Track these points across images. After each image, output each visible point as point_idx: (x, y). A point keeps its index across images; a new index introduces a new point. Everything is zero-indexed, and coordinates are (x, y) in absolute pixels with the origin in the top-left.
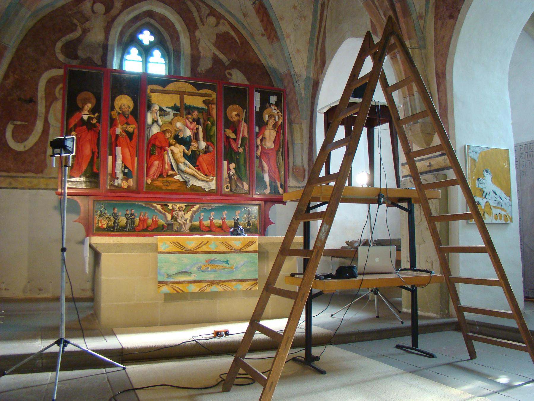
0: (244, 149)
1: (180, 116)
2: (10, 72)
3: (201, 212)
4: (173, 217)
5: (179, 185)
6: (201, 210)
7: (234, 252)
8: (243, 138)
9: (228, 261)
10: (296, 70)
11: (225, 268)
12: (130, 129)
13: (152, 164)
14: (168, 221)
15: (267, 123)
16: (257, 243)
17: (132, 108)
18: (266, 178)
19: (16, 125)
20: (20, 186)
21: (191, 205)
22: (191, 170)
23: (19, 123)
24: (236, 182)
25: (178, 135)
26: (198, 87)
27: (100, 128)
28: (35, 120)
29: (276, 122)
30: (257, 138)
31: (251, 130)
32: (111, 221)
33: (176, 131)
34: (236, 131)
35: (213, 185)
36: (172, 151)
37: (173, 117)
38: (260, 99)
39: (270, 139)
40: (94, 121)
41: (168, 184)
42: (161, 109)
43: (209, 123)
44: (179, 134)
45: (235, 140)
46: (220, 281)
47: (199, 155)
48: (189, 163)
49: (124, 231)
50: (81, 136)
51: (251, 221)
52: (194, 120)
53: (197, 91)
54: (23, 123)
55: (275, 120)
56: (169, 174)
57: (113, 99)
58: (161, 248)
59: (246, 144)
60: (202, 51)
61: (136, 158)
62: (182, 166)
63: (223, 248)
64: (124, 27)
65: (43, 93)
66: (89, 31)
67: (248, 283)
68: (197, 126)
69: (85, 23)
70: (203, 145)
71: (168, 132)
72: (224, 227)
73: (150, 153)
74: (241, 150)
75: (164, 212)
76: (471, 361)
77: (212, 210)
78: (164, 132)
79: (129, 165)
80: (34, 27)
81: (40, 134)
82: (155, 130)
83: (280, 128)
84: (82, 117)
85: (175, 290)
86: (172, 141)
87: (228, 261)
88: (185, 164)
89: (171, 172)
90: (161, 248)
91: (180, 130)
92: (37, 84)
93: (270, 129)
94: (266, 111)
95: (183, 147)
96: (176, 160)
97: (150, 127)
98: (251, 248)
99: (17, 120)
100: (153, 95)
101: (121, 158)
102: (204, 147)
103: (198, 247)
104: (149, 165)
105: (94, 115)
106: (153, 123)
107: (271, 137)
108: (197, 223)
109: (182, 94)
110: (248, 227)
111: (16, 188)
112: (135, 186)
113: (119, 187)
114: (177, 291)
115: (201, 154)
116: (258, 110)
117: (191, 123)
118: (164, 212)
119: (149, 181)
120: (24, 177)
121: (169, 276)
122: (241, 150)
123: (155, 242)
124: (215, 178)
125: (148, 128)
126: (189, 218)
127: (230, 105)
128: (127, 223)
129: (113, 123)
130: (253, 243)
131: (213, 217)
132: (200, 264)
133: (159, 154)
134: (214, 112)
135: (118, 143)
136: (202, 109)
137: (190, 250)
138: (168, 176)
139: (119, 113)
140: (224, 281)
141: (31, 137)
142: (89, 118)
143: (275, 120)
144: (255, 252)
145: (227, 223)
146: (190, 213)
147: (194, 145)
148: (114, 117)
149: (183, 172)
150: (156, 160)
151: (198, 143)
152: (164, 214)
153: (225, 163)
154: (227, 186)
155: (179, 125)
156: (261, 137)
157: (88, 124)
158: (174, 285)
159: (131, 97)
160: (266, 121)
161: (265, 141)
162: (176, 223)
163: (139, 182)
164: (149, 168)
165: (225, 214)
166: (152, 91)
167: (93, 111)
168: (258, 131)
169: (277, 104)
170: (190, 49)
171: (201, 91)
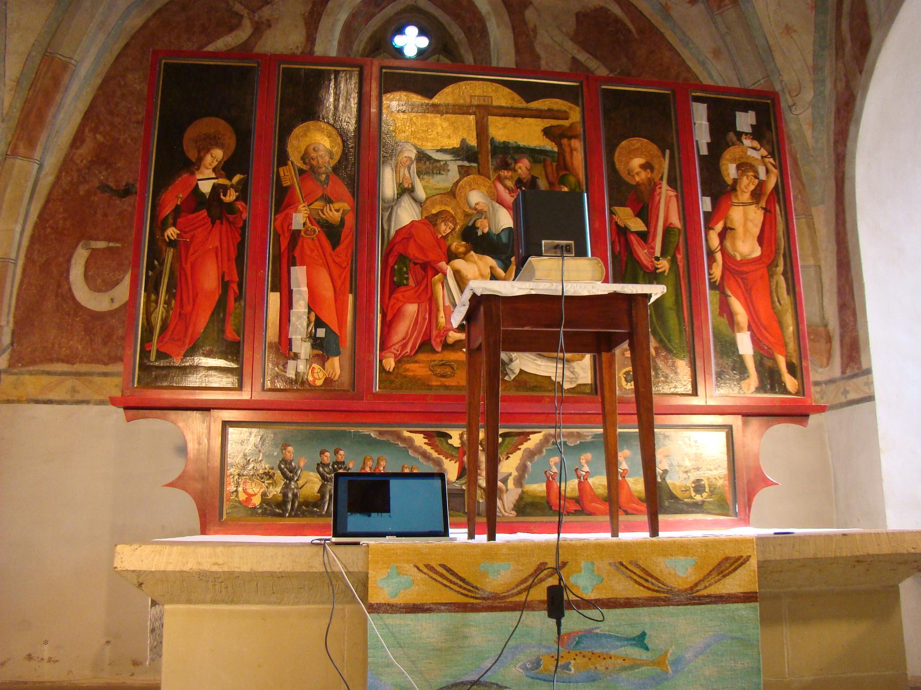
0: (674, 262)
1: (479, 173)
2: (87, 130)
3: (551, 453)
6: (550, 446)
7: (667, 602)
9: (643, 635)
10: (785, 78)
11: (635, 665)
12: (333, 214)
15: (734, 187)
16: (753, 563)
17: (337, 158)
18: (745, 344)
19: (93, 250)
20: (96, 397)
23: (101, 245)
26: (528, 92)
27: (245, 215)
29: (761, 185)
30: (708, 228)
31: (688, 208)
32: (274, 484)
33: (467, 215)
34: (645, 211)
36: (457, 274)
38: (709, 120)
39: (746, 230)
40: (231, 196)
41: (448, 371)
42: (422, 157)
44: (478, 224)
49: (313, 514)
50: (192, 238)
53: (524, 105)
54: (111, 244)
55: (756, 177)
56: (450, 340)
57: (285, 132)
58: (383, 589)
59: (677, 248)
60: (543, 55)
61: (351, 297)
63: (623, 588)
64: (354, 16)
66: (270, 26)
69: (260, 8)
73: (392, 281)
75: (435, 455)
78: (431, 221)
79: (330, 318)
80: (145, 26)
82: (407, 215)
83: (776, 201)
84: (197, 185)
86: (457, 245)
87: (643, 635)
90: (383, 589)
91: (481, 213)
93: (744, 204)
94: (728, 154)
97: (391, 206)
98: (733, 584)
99: (96, 240)
101: (306, 296)
105: (230, 180)
107: (750, 224)
108: (538, 488)
109: (483, 112)
111: (87, 402)
112: (346, 379)
113: (300, 382)
116: (704, 151)
118: (435, 455)
119: (390, 363)
120: (105, 374)
123: (357, 567)
126: (515, 473)
127: (625, 137)
128: (322, 490)
129: (284, 199)
130: (738, 562)
133: (418, 283)
134: (578, 160)
135: (297, 253)
136: (543, 152)
137: (495, 597)
138: (446, 346)
139: (301, 172)
143: (756, 177)
144: (748, 598)
148: (286, 183)
154: (627, 373)
155: (476, 198)
156: (719, 227)
157: (213, 205)
160: (730, 182)
161: (734, 239)
163: (360, 366)
164: (388, 326)
167: (226, 169)
168: (709, 209)
169: (758, 133)
170: (513, 51)
171: (535, 105)
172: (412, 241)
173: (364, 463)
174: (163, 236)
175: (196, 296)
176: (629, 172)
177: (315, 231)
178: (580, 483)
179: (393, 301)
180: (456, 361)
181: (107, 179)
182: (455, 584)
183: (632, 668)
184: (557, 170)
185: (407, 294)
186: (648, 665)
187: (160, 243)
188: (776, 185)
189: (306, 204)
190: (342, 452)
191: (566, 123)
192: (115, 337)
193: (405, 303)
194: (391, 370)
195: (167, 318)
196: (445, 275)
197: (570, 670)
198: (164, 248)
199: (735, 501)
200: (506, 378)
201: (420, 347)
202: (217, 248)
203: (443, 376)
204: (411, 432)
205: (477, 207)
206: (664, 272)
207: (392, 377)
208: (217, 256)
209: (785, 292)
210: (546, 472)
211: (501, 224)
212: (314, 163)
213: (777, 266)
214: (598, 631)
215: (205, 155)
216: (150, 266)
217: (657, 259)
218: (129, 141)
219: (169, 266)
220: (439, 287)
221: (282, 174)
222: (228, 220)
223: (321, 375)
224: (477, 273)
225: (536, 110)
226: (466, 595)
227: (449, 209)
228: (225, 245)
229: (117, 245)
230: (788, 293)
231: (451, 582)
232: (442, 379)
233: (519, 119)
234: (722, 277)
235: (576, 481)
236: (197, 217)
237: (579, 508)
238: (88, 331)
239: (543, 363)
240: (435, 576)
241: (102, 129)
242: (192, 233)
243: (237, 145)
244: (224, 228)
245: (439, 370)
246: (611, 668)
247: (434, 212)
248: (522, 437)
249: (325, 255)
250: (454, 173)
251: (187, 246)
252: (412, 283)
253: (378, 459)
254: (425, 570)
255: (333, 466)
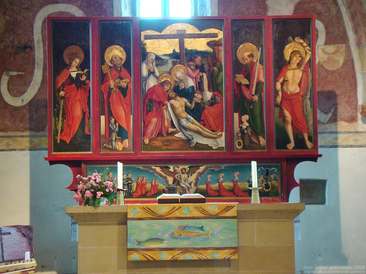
3: (208, 174)
4: (174, 181)
5: (181, 143)
7: (210, 218)
8: (259, 83)
9: (202, 227)
12: (123, 84)
13: (149, 122)
14: (169, 185)
17: (124, 61)
20: (19, 147)
21: (196, 167)
22: (194, 125)
23: (14, 73)
24: (249, 137)
25: (178, 87)
28: (33, 69)
29: (303, 59)
33: (176, 82)
35: (222, 142)
36: (172, 105)
37: (172, 66)
40: (84, 78)
41: (169, 143)
43: (216, 68)
44: (180, 85)
45: (248, 86)
46: (195, 249)
47: (204, 108)
48: (192, 118)
50: (70, 95)
51: (269, 183)
52: (197, 67)
53: (199, 32)
54: (20, 73)
56: (169, 132)
59: (262, 90)
62: (184, 122)
65: (40, 36)
67: (226, 251)
68: (201, 74)
70: (208, 95)
71: (167, 84)
72: (236, 191)
73: (147, 109)
74: (256, 98)
75: (164, 175)
76: (126, 261)
77: (221, 171)
81: (39, 85)
82: (152, 83)
85: (146, 257)
87: (202, 227)
88: (187, 119)
89: (171, 130)
91: (181, 80)
92: (32, 26)
93: (293, 69)
95: (185, 100)
96: (177, 116)
98: (228, 214)
100: (148, 42)
102: (209, 98)
103: (170, 213)
104: (146, 123)
105: (83, 72)
106: (149, 75)
107: (295, 78)
110: (267, 190)
111: (15, 150)
114: (147, 259)
115: (206, 106)
117: (193, 70)
118: (164, 175)
120: (22, 136)
121: (139, 243)
122: (256, 98)
124: (224, 133)
125: (144, 81)
126: (194, 181)
131: (222, 179)
132: (173, 231)
133: (157, 110)
137: (162, 216)
138: (168, 134)
139: (110, 67)
140: (198, 249)
141: (29, 90)
142: (78, 75)
144: (234, 217)
145: (240, 187)
146: (194, 176)
147: (198, 96)
149: (186, 129)
150: (154, 117)
151: (202, 94)
152: (165, 178)
153: (236, 115)
156: (281, 80)
157: (78, 82)
158: (145, 252)
159: (123, 48)
161: (287, 85)
162: (179, 187)
164: (146, 127)
165: (222, 176)
166: (147, 37)
171: (204, 32)
172: (154, 92)
173: (138, 178)
174: (59, 95)
175: (73, 117)
176: (243, 59)
177: (117, 91)
178: (219, 185)
179: (147, 117)
180: (172, 140)
181: (14, 39)
182: (150, 212)
183: (199, 236)
184: (213, 60)
185: (153, 115)
186: (204, 235)
187: (58, 98)
188: (310, 59)
189: (113, 80)
190: (130, 175)
191: (217, 39)
192: (25, 118)
193: (152, 118)
194: (147, 144)
195: (63, 127)
196: (167, 106)
197: (182, 236)
198: (59, 99)
199: (282, 192)
200: (191, 146)
201: (158, 135)
202: (80, 99)
203: (167, 145)
204: (155, 166)
205: (179, 78)
206: (256, 101)
207: (148, 146)
208: (80, 101)
209: (310, 107)
210: (206, 181)
211: (189, 84)
212: (115, 63)
213: (307, 95)
214: (189, 225)
215: (72, 62)
216: (55, 107)
217: (253, 96)
218: (22, 19)
219: (62, 107)
220: (165, 111)
221: (103, 68)
222: (83, 88)
223: (121, 146)
224: (180, 105)
225: (205, 34)
226: (153, 216)
227: (169, 79)
228: (83, 97)
229: (22, 73)
230: (311, 107)
231: (149, 212)
232: (167, 147)
233: (197, 39)
234: (281, 102)
235: (218, 184)
236: (72, 87)
237: (219, 194)
238: (12, 116)
239: (205, 139)
240: (145, 210)
241: (8, 13)
242: (70, 93)
243: (85, 57)
244: (82, 91)
245: (165, 143)
246: (193, 235)
247: (163, 81)
248: (197, 168)
249: (121, 101)
250: (170, 64)
251: (68, 98)
252: (154, 110)
253: (143, 177)
254: (143, 209)
255: (127, 180)
